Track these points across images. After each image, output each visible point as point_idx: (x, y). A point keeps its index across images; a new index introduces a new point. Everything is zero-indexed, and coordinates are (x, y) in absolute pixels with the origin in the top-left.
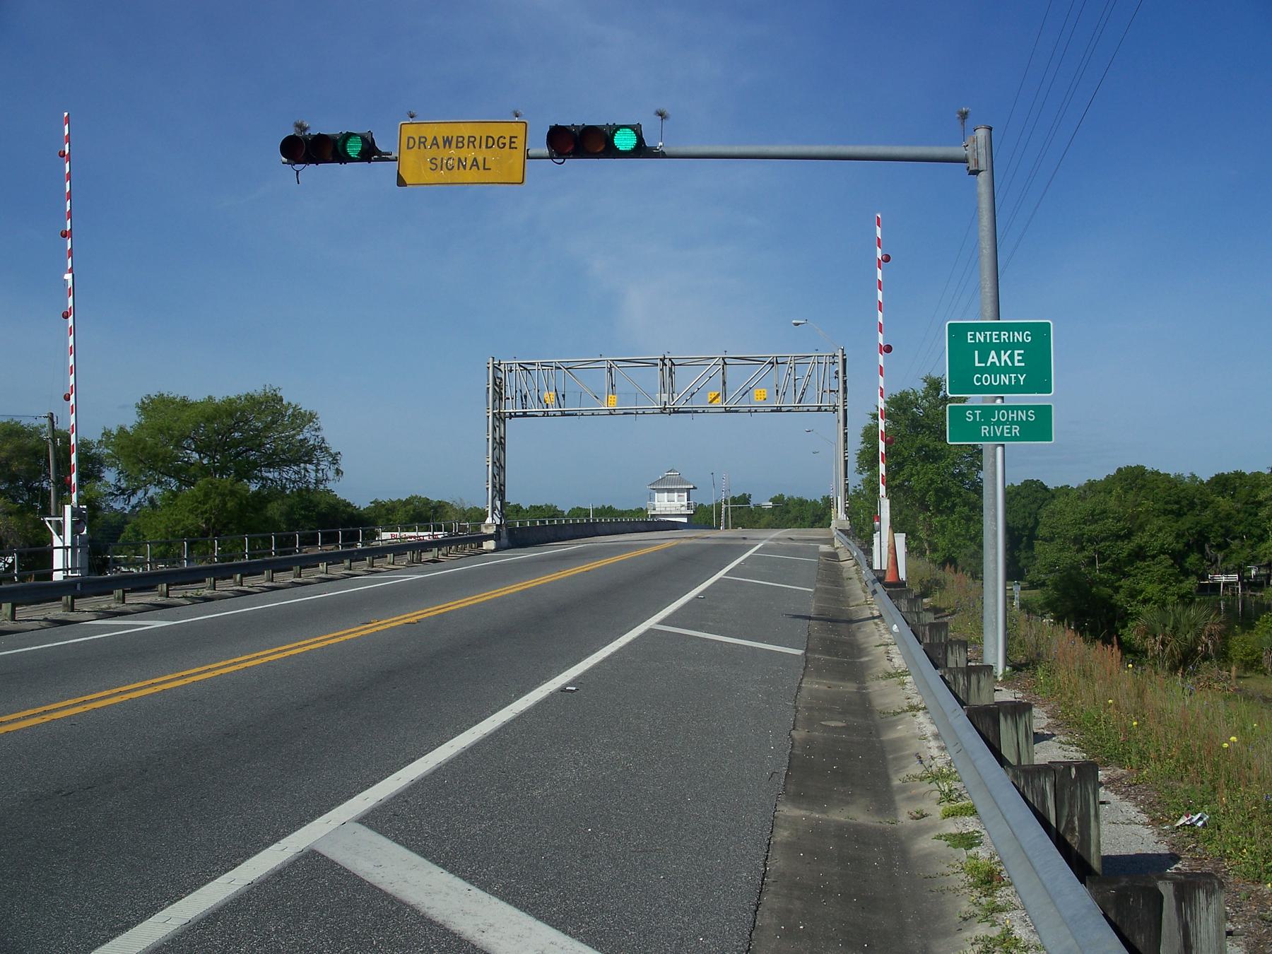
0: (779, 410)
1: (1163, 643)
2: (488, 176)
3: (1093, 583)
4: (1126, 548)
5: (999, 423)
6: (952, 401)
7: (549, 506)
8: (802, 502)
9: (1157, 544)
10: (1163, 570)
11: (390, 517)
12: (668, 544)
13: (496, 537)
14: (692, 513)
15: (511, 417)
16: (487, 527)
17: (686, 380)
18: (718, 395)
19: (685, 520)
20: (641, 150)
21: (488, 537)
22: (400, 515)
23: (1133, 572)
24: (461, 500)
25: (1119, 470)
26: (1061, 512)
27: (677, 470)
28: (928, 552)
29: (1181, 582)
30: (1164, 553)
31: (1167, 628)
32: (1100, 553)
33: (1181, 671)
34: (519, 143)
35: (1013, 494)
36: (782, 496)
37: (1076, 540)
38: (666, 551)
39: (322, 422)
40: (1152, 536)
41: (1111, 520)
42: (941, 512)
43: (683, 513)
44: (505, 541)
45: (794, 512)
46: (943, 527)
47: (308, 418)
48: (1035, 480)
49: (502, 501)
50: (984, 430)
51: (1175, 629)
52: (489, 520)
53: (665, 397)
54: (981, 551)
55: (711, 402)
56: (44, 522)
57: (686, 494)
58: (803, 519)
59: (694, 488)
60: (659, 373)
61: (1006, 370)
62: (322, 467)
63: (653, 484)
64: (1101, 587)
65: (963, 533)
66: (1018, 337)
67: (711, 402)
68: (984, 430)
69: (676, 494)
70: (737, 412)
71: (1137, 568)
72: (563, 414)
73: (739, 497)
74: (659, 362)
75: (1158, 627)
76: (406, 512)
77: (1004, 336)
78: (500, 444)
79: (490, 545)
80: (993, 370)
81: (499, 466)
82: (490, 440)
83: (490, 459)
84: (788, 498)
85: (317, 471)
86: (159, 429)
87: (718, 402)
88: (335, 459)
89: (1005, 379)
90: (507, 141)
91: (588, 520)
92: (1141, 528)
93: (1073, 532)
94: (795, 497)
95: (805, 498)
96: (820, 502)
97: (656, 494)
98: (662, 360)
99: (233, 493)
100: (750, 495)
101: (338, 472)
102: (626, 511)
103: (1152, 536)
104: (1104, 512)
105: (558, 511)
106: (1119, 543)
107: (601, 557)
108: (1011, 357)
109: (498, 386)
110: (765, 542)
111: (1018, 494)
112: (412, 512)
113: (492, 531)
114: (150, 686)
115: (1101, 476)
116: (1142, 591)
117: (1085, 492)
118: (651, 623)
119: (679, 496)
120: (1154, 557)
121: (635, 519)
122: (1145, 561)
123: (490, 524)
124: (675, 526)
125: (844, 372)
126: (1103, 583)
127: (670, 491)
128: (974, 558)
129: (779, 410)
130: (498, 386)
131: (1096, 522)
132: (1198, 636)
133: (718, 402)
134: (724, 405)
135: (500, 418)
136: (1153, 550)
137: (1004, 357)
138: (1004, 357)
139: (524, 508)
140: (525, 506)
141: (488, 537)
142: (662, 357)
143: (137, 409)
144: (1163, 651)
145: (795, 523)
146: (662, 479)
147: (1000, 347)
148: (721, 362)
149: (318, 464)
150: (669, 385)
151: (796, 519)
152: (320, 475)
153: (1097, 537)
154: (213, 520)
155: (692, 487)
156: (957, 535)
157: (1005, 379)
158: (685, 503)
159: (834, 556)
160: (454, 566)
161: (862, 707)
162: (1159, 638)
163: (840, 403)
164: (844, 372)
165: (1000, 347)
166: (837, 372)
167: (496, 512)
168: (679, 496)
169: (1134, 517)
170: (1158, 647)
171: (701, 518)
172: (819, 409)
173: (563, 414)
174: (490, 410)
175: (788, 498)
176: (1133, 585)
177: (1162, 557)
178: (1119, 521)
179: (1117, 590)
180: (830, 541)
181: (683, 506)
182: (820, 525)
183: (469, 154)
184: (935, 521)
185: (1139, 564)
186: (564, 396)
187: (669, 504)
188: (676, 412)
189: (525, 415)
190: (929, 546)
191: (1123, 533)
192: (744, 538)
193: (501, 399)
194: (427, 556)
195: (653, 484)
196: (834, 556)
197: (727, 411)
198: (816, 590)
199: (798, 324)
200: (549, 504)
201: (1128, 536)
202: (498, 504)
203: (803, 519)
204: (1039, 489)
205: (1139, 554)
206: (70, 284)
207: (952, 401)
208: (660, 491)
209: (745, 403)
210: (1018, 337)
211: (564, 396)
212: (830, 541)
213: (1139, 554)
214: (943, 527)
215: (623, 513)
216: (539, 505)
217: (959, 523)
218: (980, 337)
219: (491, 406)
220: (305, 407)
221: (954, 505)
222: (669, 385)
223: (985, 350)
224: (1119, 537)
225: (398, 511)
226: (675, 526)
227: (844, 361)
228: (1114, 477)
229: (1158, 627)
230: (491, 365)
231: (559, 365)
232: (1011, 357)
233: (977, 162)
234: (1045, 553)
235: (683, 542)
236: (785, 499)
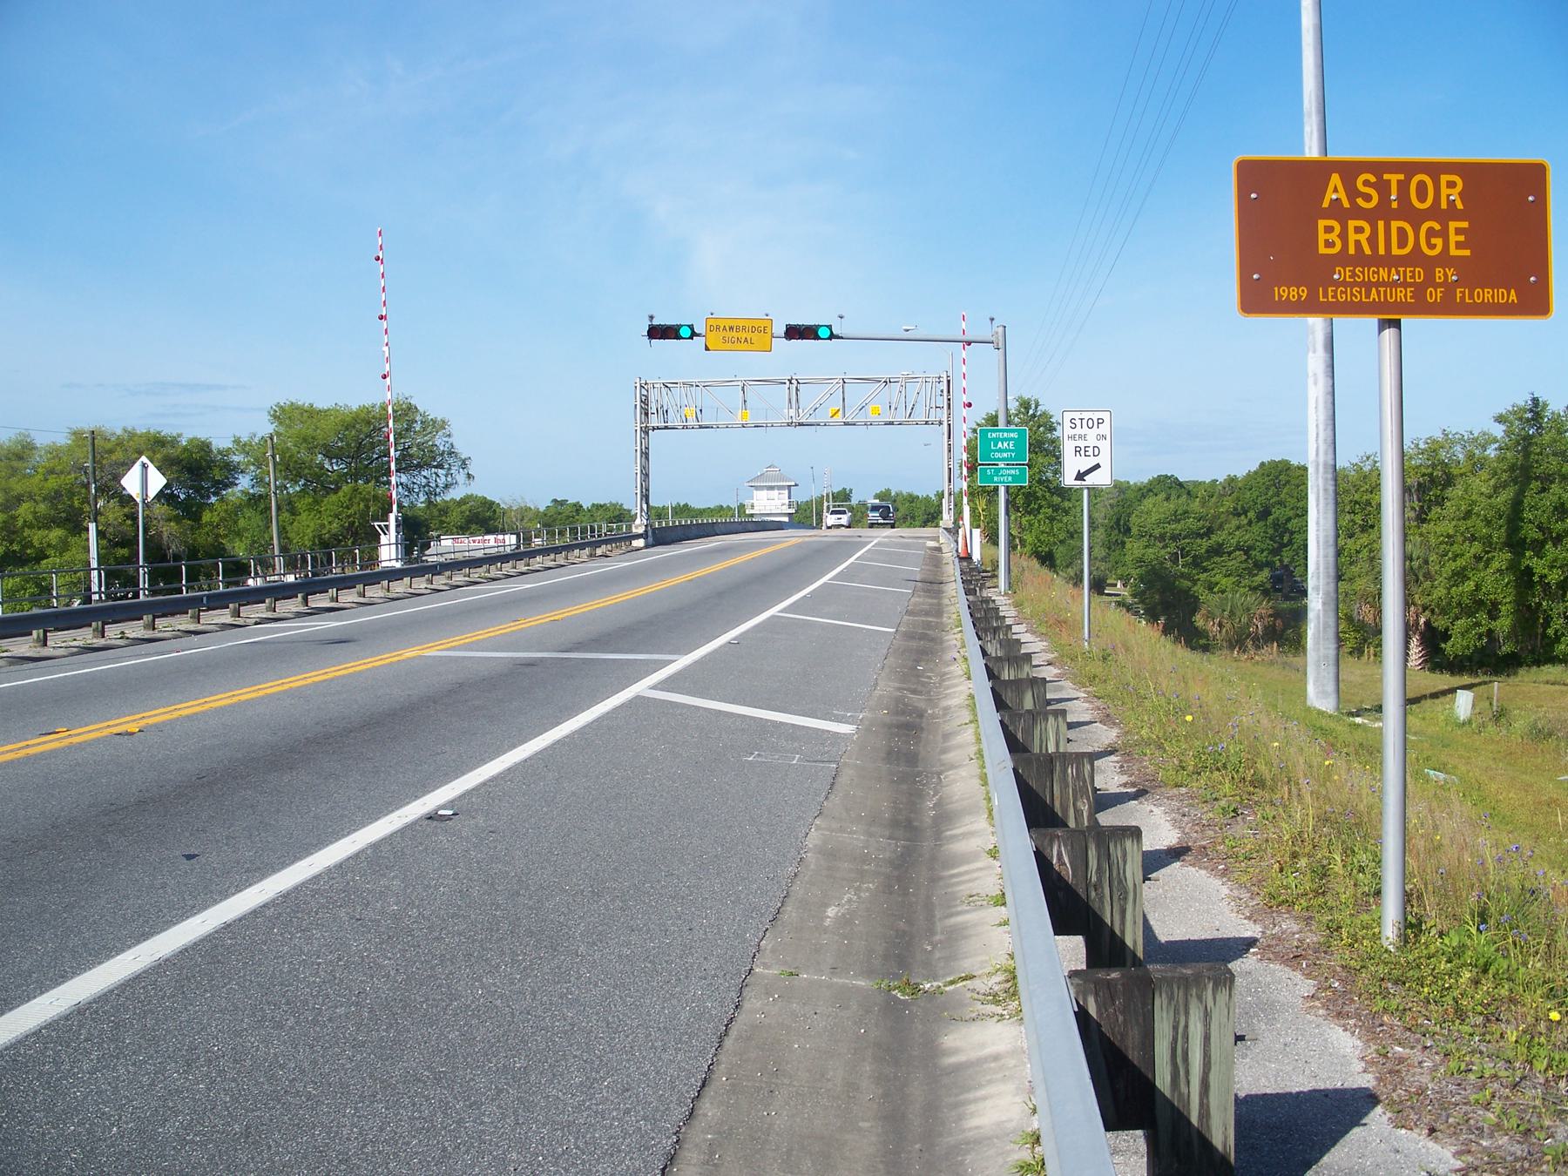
0: (891, 423)
1: (1220, 625)
2: (750, 347)
3: (1176, 577)
4: (1205, 544)
5: (1002, 475)
6: (980, 465)
7: (614, 505)
8: (912, 499)
9: (1234, 542)
10: (1238, 565)
11: (443, 518)
12: (794, 541)
13: (644, 536)
14: (794, 511)
15: (654, 429)
16: (636, 527)
17: (809, 396)
18: (839, 410)
19: (786, 519)
20: (832, 336)
21: (638, 536)
22: (455, 517)
23: (1209, 567)
24: (522, 498)
25: (1262, 464)
26: (1149, 513)
27: (776, 465)
28: (1019, 547)
29: (1256, 575)
30: (1239, 550)
31: (1226, 613)
32: (1182, 549)
33: (1237, 649)
34: (768, 330)
35: (1145, 491)
36: (888, 491)
37: (1162, 538)
38: (799, 546)
39: (454, 427)
40: (1230, 534)
41: (1191, 520)
42: (1029, 513)
43: (783, 512)
44: (650, 539)
45: (902, 511)
46: (1031, 525)
47: (439, 426)
48: (1169, 475)
49: (647, 503)
50: (996, 479)
51: (1232, 613)
52: (638, 521)
53: (792, 412)
54: (917, 523)
55: (832, 417)
56: (374, 526)
57: (786, 492)
58: (913, 518)
59: (796, 485)
60: (787, 391)
61: (1006, 451)
62: (452, 472)
63: (752, 481)
64: (1182, 580)
65: (1047, 530)
66: (1012, 435)
67: (832, 417)
68: (996, 479)
69: (776, 492)
70: (854, 425)
71: (1214, 563)
72: (701, 427)
73: (838, 492)
74: (787, 381)
75: (1217, 612)
76: (462, 513)
77: (1005, 435)
78: (645, 455)
79: (640, 543)
80: (1000, 451)
81: (645, 475)
82: (639, 451)
83: (639, 468)
84: (896, 493)
85: (446, 476)
86: (303, 439)
87: (839, 417)
88: (464, 464)
89: (1005, 455)
90: (762, 329)
91: (667, 523)
92: (1221, 527)
93: (1157, 533)
94: (904, 493)
95: (915, 493)
96: (933, 498)
97: (755, 492)
98: (790, 381)
99: (375, 497)
100: (851, 491)
101: (469, 476)
102: (704, 510)
103: (1230, 534)
104: (1186, 512)
105: (625, 510)
106: (1199, 541)
107: (760, 548)
108: (1008, 445)
109: (645, 402)
110: (878, 539)
111: (1151, 490)
112: (468, 513)
113: (641, 530)
114: (323, 674)
115: (1240, 472)
116: (1217, 584)
117: (1225, 488)
118: (852, 560)
119: (779, 494)
120: (1230, 554)
121: (692, 522)
122: (1222, 557)
123: (639, 526)
124: (779, 526)
125: (949, 392)
126: (1183, 575)
127: (771, 488)
128: (1106, 562)
129: (891, 423)
130: (645, 402)
131: (1179, 521)
132: (1250, 619)
133: (839, 417)
134: (844, 420)
135: (646, 431)
136: (1230, 547)
137: (1005, 444)
138: (1005, 444)
139: (585, 507)
140: (586, 505)
141: (638, 536)
142: (790, 378)
143: (269, 417)
144: (1220, 632)
145: (904, 522)
146: (761, 475)
147: (1006, 440)
148: (841, 381)
149: (449, 469)
150: (795, 401)
151: (905, 518)
152: (449, 479)
153: (1180, 535)
154: (357, 524)
155: (793, 484)
156: (1043, 532)
157: (1005, 455)
158: (787, 501)
159: (939, 549)
160: (618, 563)
161: (939, 604)
162: (1217, 621)
163: (945, 419)
164: (949, 392)
165: (1006, 440)
166: (942, 391)
167: (643, 514)
168: (779, 494)
169: (1216, 517)
170: (1216, 628)
171: (805, 516)
172: (927, 423)
173: (701, 427)
174: (638, 425)
175: (896, 493)
176: (1208, 578)
177: (1238, 553)
178: (1199, 521)
179: (1195, 582)
180: (936, 539)
181: (783, 505)
182: (933, 525)
183: (743, 335)
184: (1024, 521)
185: (1217, 559)
186: (701, 410)
187: (770, 503)
188: (801, 424)
189: (666, 428)
190: (1020, 542)
191: (1202, 531)
192: (860, 536)
193: (647, 414)
194: (599, 551)
195: (752, 481)
196: (939, 549)
197: (846, 424)
198: (922, 569)
199: (908, 330)
200: (614, 502)
201: (1209, 532)
202: (645, 506)
203: (913, 518)
204: (1174, 485)
205: (1217, 550)
206: (387, 355)
207: (980, 465)
208: (758, 488)
209: (860, 418)
210: (1012, 435)
211: (701, 410)
212: (936, 539)
213: (1217, 550)
214: (1031, 525)
215: (701, 512)
216: (602, 503)
217: (1045, 522)
218: (994, 435)
219: (638, 421)
220: (434, 413)
221: (1040, 507)
222: (795, 401)
223: (996, 440)
224: (1201, 536)
225: (452, 511)
226: (779, 526)
227: (949, 381)
228: (1256, 473)
229: (1217, 612)
230: (638, 385)
231: (698, 384)
232: (1008, 445)
233: (998, 344)
234: (1134, 548)
235: (807, 539)
236: (893, 494)
